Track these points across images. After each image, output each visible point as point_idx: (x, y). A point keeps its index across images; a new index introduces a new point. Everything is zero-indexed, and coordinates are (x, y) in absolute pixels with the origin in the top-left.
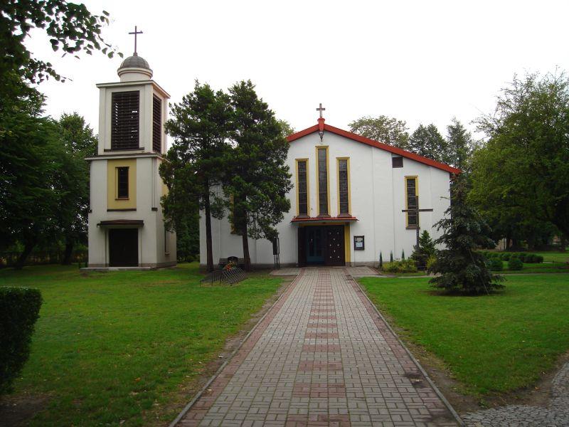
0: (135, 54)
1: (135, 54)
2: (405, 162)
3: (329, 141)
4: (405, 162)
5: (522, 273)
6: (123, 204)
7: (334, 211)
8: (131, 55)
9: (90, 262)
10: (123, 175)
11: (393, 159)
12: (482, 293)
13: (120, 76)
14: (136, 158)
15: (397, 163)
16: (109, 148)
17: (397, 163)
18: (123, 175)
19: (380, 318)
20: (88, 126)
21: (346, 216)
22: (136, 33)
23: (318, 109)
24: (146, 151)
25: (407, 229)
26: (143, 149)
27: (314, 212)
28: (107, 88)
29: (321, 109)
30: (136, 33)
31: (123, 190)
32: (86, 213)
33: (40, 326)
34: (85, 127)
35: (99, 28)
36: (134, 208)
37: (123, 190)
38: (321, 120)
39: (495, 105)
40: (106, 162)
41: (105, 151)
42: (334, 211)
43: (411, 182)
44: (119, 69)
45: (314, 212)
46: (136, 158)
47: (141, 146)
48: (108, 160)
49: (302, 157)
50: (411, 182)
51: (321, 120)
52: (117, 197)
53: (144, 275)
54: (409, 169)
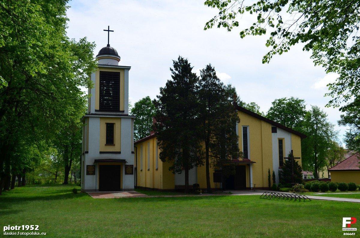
0: (108, 45)
1: (108, 45)
6: (110, 149)
10: (110, 129)
11: (272, 128)
14: (121, 118)
16: (98, 109)
17: (274, 131)
18: (110, 129)
24: (125, 113)
25: (105, 145)
31: (110, 140)
35: (202, 70)
37: (110, 140)
39: (215, 69)
40: (99, 119)
41: (96, 111)
43: (281, 142)
46: (121, 118)
47: (121, 109)
48: (101, 118)
50: (281, 142)
53: (145, 199)
54: (280, 134)
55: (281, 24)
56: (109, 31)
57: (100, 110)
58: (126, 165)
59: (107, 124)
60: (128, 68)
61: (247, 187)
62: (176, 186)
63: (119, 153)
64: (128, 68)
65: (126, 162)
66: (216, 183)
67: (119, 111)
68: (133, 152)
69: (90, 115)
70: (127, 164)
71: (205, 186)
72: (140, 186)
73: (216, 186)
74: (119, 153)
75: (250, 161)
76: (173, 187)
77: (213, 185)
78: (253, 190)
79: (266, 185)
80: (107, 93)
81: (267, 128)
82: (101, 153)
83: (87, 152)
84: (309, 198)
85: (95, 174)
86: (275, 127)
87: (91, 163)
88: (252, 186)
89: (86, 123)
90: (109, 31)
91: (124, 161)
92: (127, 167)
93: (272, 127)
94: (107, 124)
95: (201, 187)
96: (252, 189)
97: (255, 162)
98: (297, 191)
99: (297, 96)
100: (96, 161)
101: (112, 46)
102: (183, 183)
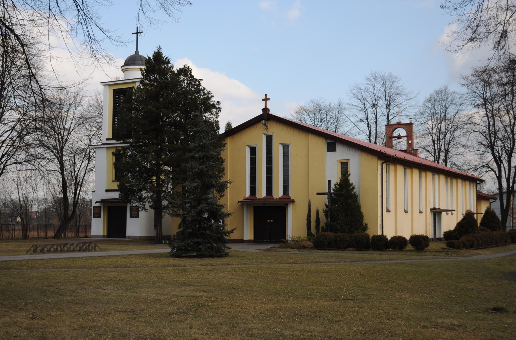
0: (137, 52)
1: (137, 52)
2: (339, 147)
3: (275, 129)
4: (339, 147)
7: (278, 192)
9: (128, 234)
12: (221, 256)
13: (123, 72)
15: (331, 148)
16: (111, 137)
17: (331, 148)
21: (253, 198)
22: (137, 33)
23: (263, 100)
27: (262, 193)
28: (109, 85)
29: (266, 99)
30: (137, 33)
32: (222, 188)
38: (266, 110)
41: (107, 139)
42: (278, 192)
43: (344, 165)
44: (122, 67)
45: (262, 193)
48: (107, 148)
49: (252, 143)
50: (344, 165)
51: (266, 110)
52: (114, 179)
57: (113, 139)
81: (321, 144)
82: (107, 191)
100: (103, 201)
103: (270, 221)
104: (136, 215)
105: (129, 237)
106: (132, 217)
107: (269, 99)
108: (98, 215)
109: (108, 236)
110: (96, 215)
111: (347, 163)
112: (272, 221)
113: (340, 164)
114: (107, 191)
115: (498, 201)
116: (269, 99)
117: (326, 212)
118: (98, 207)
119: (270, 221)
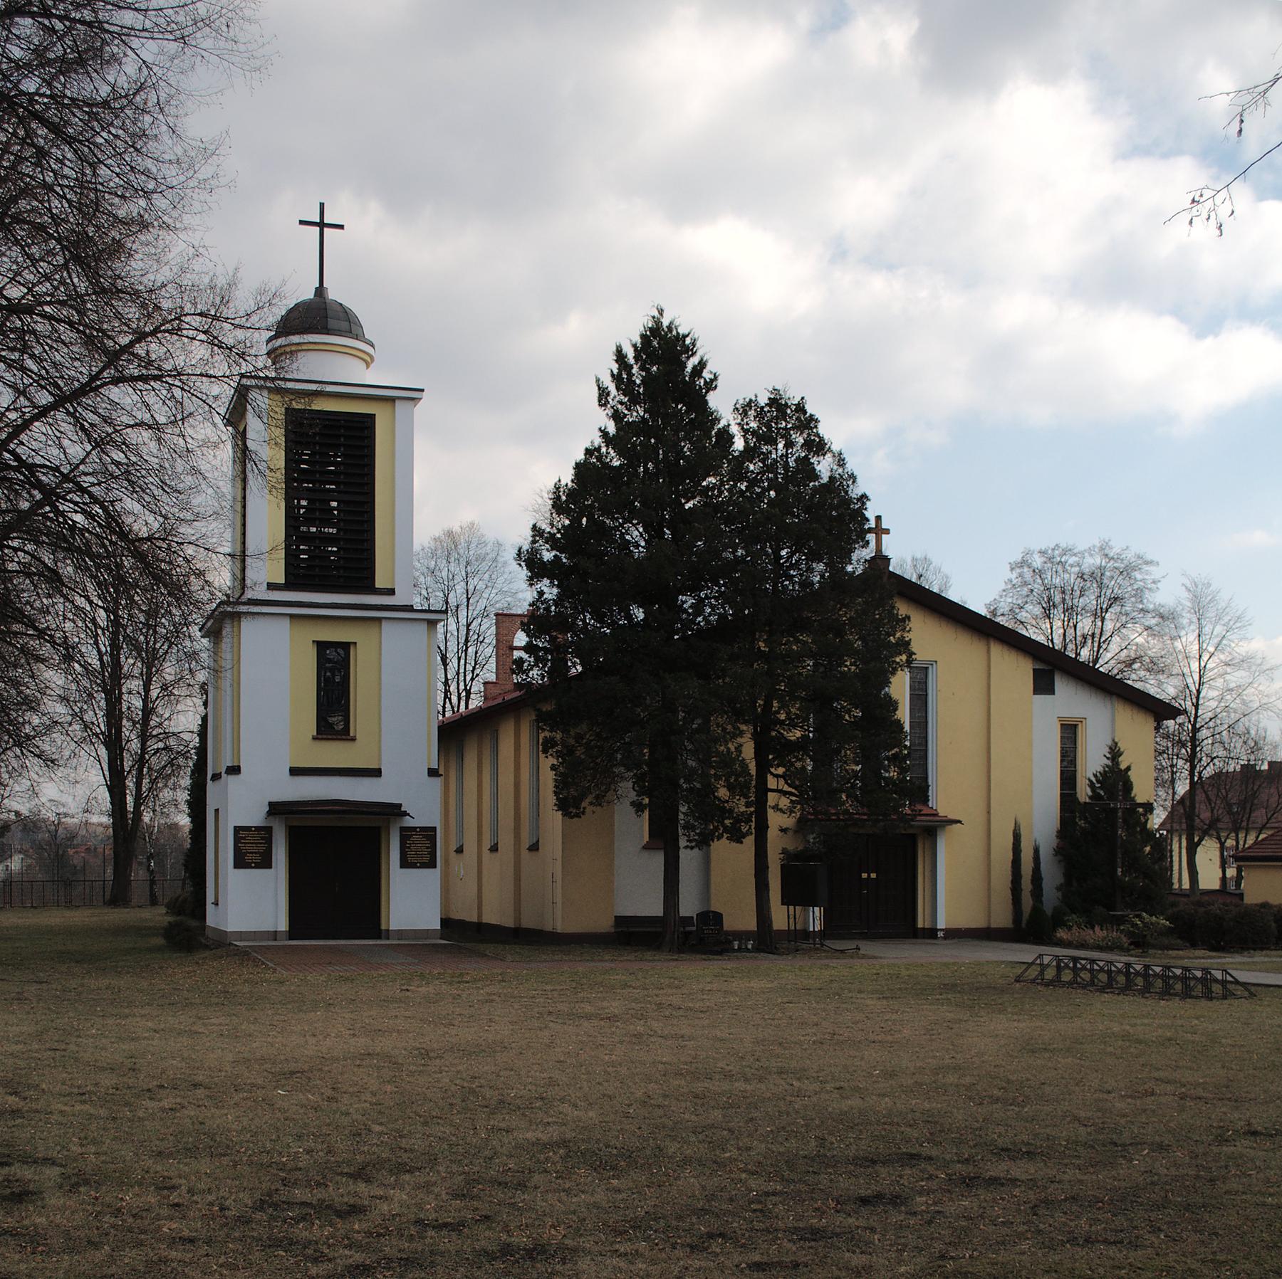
0: (320, 290)
1: (320, 290)
2: (1061, 684)
4: (1061, 684)
5: (1267, 956)
6: (334, 754)
8: (309, 295)
11: (1036, 672)
15: (1043, 685)
16: (281, 579)
17: (1043, 685)
19: (437, 1221)
20: (702, 365)
25: (314, 738)
26: (391, 592)
33: (1022, 867)
34: (692, 363)
36: (373, 765)
40: (287, 621)
41: (272, 586)
43: (1070, 731)
46: (379, 620)
47: (379, 584)
48: (292, 616)
50: (1070, 731)
55: (780, 807)
56: (322, 225)
57: (289, 585)
58: (403, 829)
59: (321, 646)
60: (412, 395)
61: (920, 925)
62: (620, 920)
63: (376, 773)
64: (412, 395)
65: (405, 814)
66: (791, 908)
67: (371, 589)
68: (433, 773)
69: (244, 604)
70: (408, 822)
71: (749, 922)
72: (452, 917)
73: (792, 920)
74: (376, 773)
75: (936, 815)
76: (604, 924)
77: (780, 917)
78: (945, 938)
79: (1002, 919)
80: (342, 533)
81: (1019, 671)
82: (295, 772)
83: (234, 770)
84: (1241, 980)
85: (270, 867)
86: (1050, 668)
87: (254, 816)
88: (941, 924)
89: (226, 643)
90: (322, 225)
91: (394, 811)
92: (407, 834)
93: (1034, 670)
94: (321, 646)
95: (729, 924)
96: (940, 934)
97: (960, 822)
98: (1139, 943)
99: (1127, 543)
100: (275, 809)
101: (333, 294)
102: (654, 908)
103: (869, 876)
104: (426, 860)
105: (401, 934)
106: (405, 864)
107: (887, 531)
108: (258, 859)
109: (294, 932)
110: (248, 858)
111: (1076, 726)
112: (864, 875)
113: (1059, 726)
114: (295, 772)
115: (750, 841)
116: (887, 531)
117: (1059, 851)
118: (258, 828)
119: (869, 876)
